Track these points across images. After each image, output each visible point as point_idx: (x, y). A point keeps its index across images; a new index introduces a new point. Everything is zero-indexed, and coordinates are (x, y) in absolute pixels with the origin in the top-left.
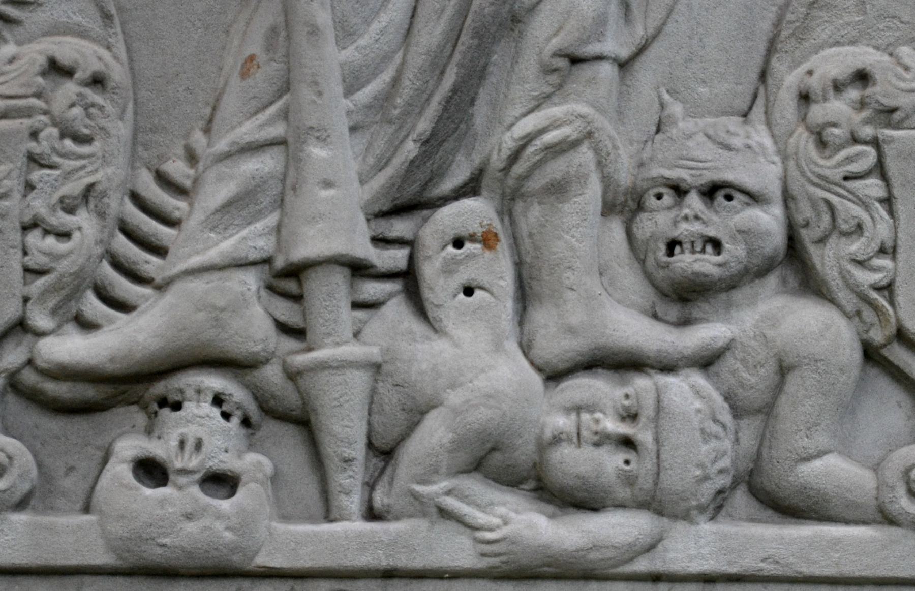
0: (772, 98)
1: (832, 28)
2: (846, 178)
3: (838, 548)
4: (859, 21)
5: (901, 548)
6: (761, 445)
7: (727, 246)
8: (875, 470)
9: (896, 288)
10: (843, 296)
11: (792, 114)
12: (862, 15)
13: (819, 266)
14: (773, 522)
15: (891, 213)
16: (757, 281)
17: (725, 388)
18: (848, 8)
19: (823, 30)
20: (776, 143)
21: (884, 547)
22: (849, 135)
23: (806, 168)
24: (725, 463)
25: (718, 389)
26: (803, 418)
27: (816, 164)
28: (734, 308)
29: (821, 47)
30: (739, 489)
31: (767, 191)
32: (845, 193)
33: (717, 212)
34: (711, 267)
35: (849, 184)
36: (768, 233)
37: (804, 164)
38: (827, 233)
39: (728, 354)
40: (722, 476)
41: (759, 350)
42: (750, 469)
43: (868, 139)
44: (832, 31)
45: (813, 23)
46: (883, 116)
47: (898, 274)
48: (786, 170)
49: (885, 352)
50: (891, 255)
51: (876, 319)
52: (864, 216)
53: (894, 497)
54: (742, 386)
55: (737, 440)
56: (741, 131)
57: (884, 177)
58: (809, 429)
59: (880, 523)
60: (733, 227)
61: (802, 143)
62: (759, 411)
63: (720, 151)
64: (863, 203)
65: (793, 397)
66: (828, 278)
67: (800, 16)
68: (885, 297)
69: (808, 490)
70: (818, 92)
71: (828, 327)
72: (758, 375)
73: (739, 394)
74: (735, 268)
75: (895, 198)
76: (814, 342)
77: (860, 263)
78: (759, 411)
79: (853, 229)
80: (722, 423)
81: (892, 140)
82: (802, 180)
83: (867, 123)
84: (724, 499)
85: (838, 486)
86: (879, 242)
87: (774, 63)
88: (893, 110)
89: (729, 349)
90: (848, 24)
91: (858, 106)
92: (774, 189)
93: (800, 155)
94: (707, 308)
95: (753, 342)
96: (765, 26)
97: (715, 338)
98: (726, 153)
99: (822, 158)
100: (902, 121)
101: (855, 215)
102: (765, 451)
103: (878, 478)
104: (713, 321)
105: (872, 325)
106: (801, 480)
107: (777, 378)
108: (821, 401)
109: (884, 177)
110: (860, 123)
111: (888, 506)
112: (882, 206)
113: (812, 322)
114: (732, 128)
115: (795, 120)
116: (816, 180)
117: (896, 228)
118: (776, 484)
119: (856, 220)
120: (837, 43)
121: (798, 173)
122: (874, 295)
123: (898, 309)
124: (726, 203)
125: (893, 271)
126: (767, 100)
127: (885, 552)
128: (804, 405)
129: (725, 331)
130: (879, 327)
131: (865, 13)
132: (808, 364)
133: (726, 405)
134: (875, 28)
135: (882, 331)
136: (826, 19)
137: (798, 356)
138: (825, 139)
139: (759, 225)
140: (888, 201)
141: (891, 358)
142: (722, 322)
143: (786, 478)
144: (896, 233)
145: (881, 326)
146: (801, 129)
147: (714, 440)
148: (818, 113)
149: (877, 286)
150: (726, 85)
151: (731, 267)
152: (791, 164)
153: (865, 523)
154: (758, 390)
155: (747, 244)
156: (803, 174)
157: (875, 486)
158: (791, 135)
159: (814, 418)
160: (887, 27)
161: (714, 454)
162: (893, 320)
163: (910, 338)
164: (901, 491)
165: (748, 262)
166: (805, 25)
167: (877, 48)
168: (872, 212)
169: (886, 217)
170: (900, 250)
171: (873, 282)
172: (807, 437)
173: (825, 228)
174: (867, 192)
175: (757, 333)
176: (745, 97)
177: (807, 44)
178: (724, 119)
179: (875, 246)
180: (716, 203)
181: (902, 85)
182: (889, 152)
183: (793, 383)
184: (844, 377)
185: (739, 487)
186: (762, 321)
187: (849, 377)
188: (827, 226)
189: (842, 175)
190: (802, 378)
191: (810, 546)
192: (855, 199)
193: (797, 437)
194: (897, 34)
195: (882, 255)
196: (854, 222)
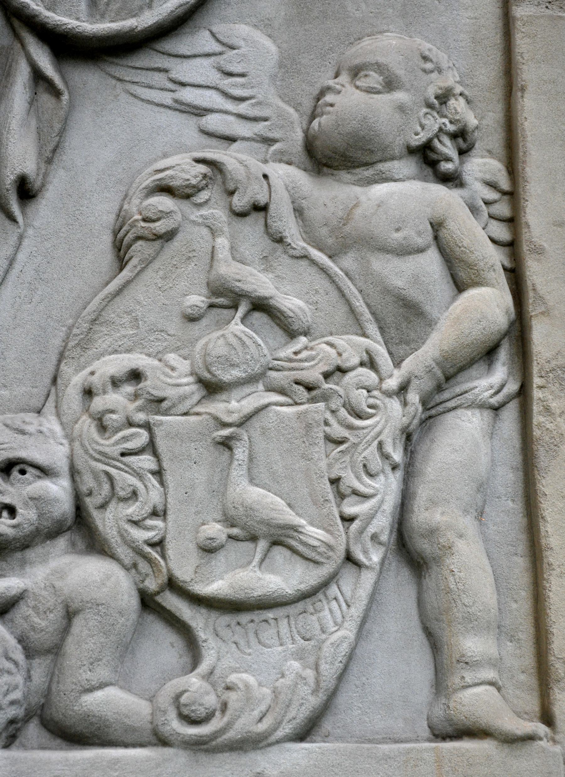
0: (61, 394)
1: (111, 339)
2: (123, 455)
3: (117, 767)
4: (133, 334)
5: (172, 765)
6: (51, 681)
7: (20, 511)
8: (151, 701)
9: (167, 543)
10: (122, 552)
11: (77, 405)
12: (136, 329)
13: (101, 528)
14: (61, 749)
15: (162, 483)
16: (48, 542)
17: (19, 632)
18: (124, 324)
19: (104, 341)
20: (64, 429)
21: (158, 765)
22: (124, 419)
23: (89, 447)
24: (17, 695)
25: (12, 633)
26: (86, 654)
27: (97, 443)
28: (28, 565)
29: (103, 355)
30: (33, 722)
31: (55, 466)
32: (123, 466)
33: (12, 485)
34: (6, 528)
35: (126, 459)
36: (56, 500)
37: (87, 443)
38: (107, 500)
39: (22, 602)
40: (14, 707)
41: (49, 598)
42: (41, 703)
43: (141, 422)
44: (111, 342)
45: (96, 336)
46: (154, 405)
47: (168, 531)
48: (72, 450)
49: (159, 599)
50: (162, 517)
51: (151, 570)
52: (139, 485)
53: (166, 719)
54: (33, 629)
55: (29, 678)
56: (35, 422)
57: (155, 454)
58: (91, 664)
59: (155, 745)
60: (26, 495)
61: (85, 428)
62: (48, 651)
63: (16, 435)
64: (138, 474)
65: (78, 636)
66: (109, 537)
67: (84, 330)
68: (157, 552)
69: (90, 718)
70: (98, 386)
71: (108, 577)
72: (47, 620)
73: (31, 637)
74: (27, 529)
75: (165, 470)
76: (96, 589)
77: (136, 523)
78: (48, 651)
79: (129, 495)
80: (14, 661)
81: (161, 423)
82: (86, 457)
83: (140, 410)
84: (18, 730)
85: (118, 713)
86: (151, 505)
87: (63, 367)
88: (161, 400)
89: (22, 598)
90: (124, 336)
91: (132, 398)
92: (62, 465)
93: (84, 437)
94: (4, 566)
95: (43, 592)
96: (57, 342)
97: (10, 588)
98: (20, 437)
99: (103, 439)
100: (170, 408)
101: (131, 484)
102: (54, 687)
103: (153, 705)
104: (9, 576)
105: (147, 575)
106: (85, 708)
107: (64, 622)
108: (102, 640)
109: (155, 454)
110: (134, 410)
111: (161, 728)
112: (154, 478)
113: (95, 573)
114: (27, 420)
115: (80, 410)
116: (97, 456)
117: (166, 494)
118: (63, 714)
119: (132, 488)
120: (116, 352)
121: (82, 451)
122: (148, 549)
123: (169, 561)
124: (21, 476)
125: (164, 530)
126: (57, 396)
127: (159, 770)
128: (87, 643)
129: (18, 583)
130: (153, 577)
131: (138, 327)
132: (91, 608)
133: (19, 647)
134: (146, 340)
135: (155, 580)
136: (106, 332)
137: (82, 601)
138: (105, 423)
139: (48, 493)
140: (159, 473)
141: (164, 604)
142: (17, 577)
143: (71, 708)
144: (166, 499)
145: (155, 577)
146: (85, 417)
147: (6, 675)
148: (98, 403)
149: (150, 542)
150: (24, 388)
151: (24, 528)
152: (77, 444)
153: (142, 745)
154: (47, 632)
155: (37, 508)
156: (86, 451)
157: (151, 712)
158: (76, 422)
159: (96, 654)
160: (156, 339)
161: (6, 688)
162: (164, 570)
163: (179, 586)
164: (172, 715)
165: (39, 523)
166: (89, 337)
167: (149, 355)
168: (145, 482)
169: (158, 485)
170: (169, 512)
171: (147, 538)
172: (90, 671)
173: (106, 495)
174: (140, 465)
175: (47, 584)
176: (40, 397)
177: (90, 352)
178: (22, 415)
179: (148, 509)
180: (12, 477)
181: (169, 380)
182: (159, 433)
183: (78, 624)
184: (123, 619)
185: (32, 720)
186: (52, 574)
187: (128, 620)
188: (107, 494)
189: (119, 451)
190: (85, 619)
191: (91, 766)
192: (130, 471)
193: (81, 671)
194: (165, 344)
195: (154, 517)
196: (130, 489)
